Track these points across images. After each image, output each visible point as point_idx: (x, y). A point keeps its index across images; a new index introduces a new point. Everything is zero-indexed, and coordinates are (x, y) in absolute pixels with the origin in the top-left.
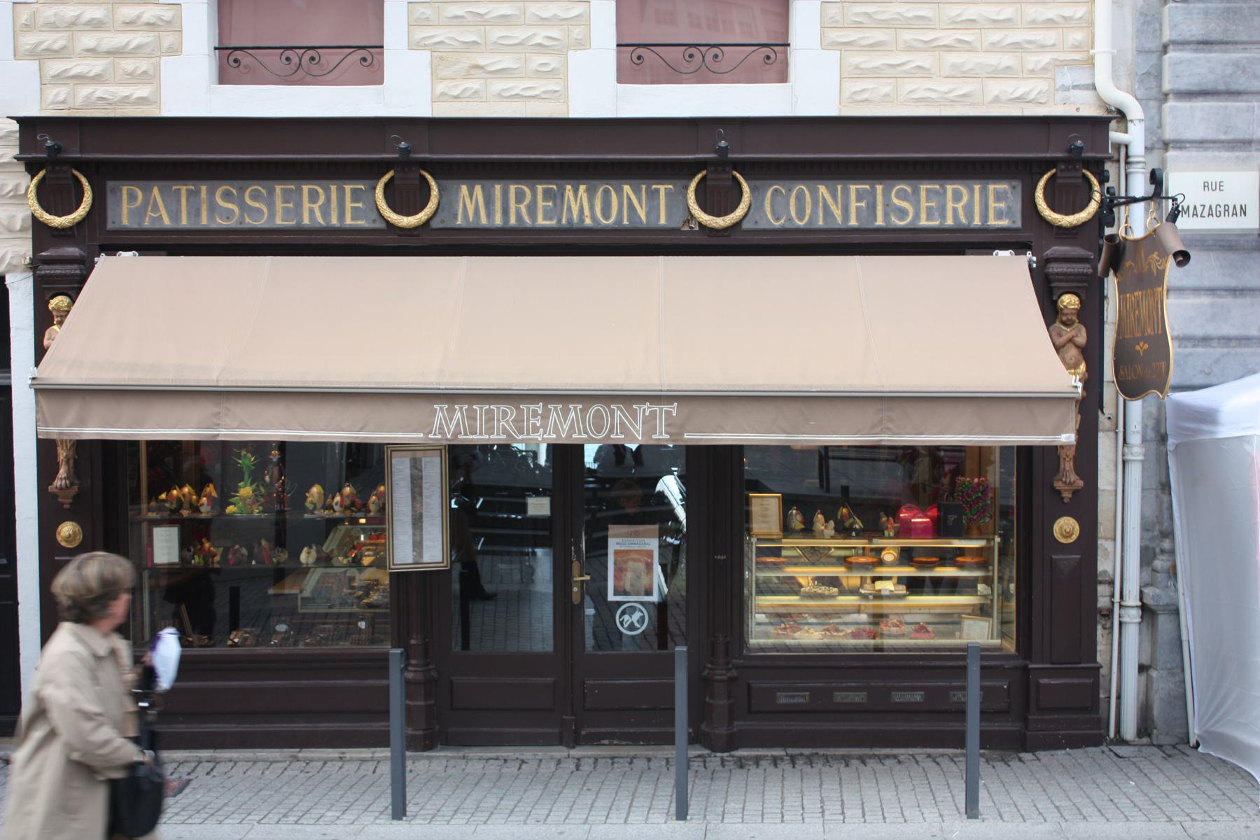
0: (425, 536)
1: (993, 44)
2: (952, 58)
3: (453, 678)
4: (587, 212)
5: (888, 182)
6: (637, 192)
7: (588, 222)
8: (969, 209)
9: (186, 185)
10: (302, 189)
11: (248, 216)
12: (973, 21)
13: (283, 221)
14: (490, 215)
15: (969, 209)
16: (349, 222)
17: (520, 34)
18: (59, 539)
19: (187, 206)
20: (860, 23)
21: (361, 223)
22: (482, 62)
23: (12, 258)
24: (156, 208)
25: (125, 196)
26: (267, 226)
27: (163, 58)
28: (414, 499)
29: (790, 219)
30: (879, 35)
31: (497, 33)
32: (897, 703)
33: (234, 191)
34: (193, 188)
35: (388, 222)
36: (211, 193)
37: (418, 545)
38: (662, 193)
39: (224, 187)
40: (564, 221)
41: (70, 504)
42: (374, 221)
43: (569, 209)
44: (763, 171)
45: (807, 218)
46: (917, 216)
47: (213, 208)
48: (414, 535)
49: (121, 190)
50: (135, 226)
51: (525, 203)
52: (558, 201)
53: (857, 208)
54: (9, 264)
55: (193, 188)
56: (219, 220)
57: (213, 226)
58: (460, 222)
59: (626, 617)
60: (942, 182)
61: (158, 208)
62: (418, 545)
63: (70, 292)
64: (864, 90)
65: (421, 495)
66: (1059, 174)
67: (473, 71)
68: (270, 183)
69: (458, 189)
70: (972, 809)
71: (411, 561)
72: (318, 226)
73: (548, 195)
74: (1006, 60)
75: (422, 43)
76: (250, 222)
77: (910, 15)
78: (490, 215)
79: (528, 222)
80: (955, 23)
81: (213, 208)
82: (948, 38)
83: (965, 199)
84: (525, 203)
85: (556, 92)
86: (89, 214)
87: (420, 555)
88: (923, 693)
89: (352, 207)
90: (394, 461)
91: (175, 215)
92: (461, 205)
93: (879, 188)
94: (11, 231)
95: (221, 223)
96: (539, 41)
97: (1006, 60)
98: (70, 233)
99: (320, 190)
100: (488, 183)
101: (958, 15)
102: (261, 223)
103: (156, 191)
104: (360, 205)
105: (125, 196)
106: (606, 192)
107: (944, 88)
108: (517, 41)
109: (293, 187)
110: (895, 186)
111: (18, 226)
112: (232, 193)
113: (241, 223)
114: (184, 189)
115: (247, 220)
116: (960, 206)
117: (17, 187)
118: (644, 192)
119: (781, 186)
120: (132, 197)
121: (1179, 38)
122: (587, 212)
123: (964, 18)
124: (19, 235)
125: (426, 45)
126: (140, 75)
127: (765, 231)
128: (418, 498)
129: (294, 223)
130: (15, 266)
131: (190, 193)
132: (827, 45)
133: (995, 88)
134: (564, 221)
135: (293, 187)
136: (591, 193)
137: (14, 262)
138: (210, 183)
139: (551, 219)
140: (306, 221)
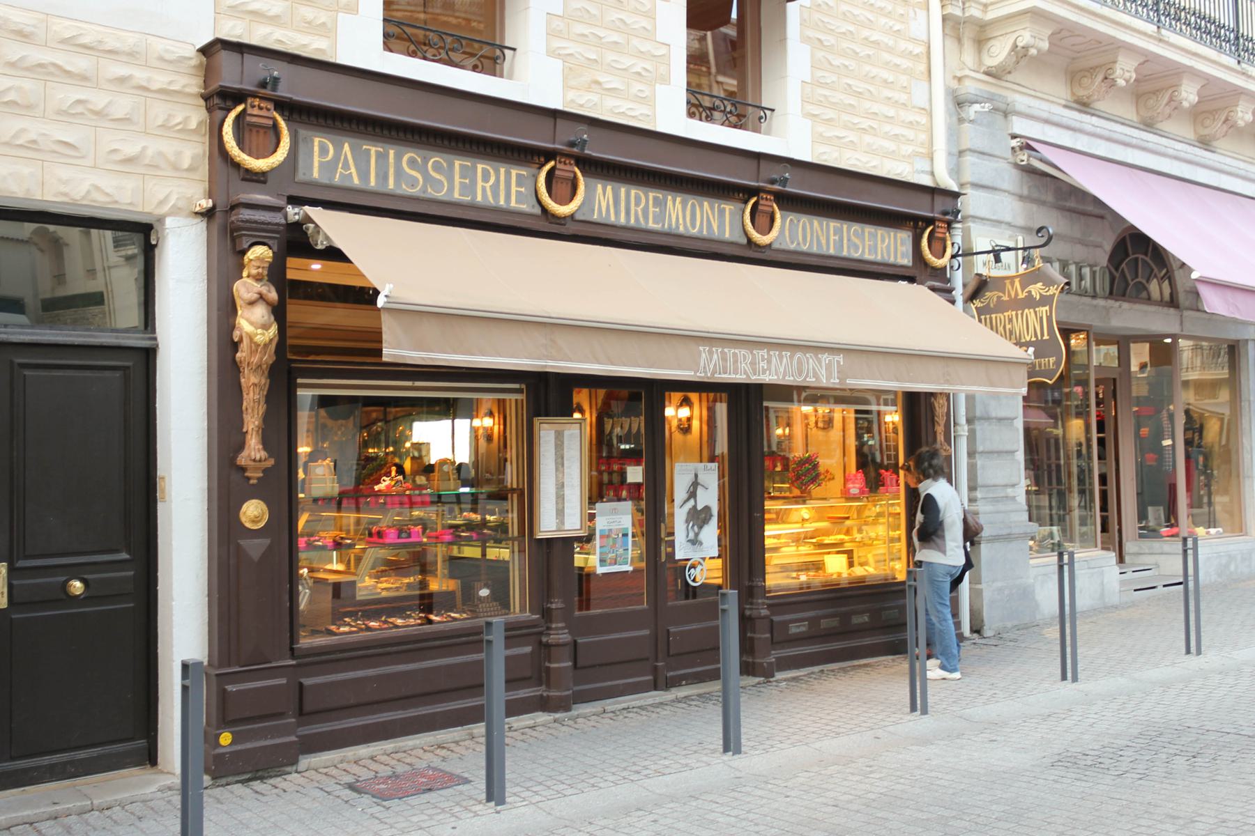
0: (566, 505)
1: (886, 133)
2: (868, 139)
3: (302, 680)
4: (681, 221)
5: (850, 223)
6: (712, 208)
7: (681, 229)
8: (495, 188)
9: (376, 146)
10: (476, 168)
11: (431, 187)
12: (876, 114)
13: (460, 195)
14: (617, 213)
15: (495, 188)
16: (513, 204)
17: (626, 62)
18: (243, 519)
19: (376, 168)
20: (821, 101)
21: (524, 207)
22: (601, 79)
23: (178, 199)
24: (346, 166)
25: (316, 149)
26: (446, 199)
27: (340, 14)
28: (557, 469)
29: (798, 244)
30: (831, 114)
31: (610, 57)
32: (856, 624)
33: (419, 160)
34: (381, 150)
35: (544, 210)
36: (398, 158)
37: (560, 513)
38: (727, 213)
39: (409, 154)
40: (666, 226)
41: (258, 479)
42: (533, 206)
43: (670, 215)
44: (792, 202)
45: (808, 244)
46: (451, 189)
47: (399, 172)
48: (557, 503)
49: (313, 142)
50: (325, 181)
51: (641, 207)
52: (663, 208)
53: (834, 240)
54: (173, 206)
55: (381, 150)
56: (404, 187)
57: (399, 192)
58: (595, 217)
59: (692, 570)
60: (473, 160)
61: (349, 165)
62: (560, 513)
63: (270, 242)
64: (825, 153)
65: (563, 465)
66: (559, 166)
67: (594, 86)
68: (451, 157)
69: (596, 187)
70: (731, 743)
71: (554, 529)
72: (489, 204)
73: (657, 202)
74: (891, 146)
75: (557, 53)
76: (431, 193)
77: (847, 102)
78: (617, 213)
79: (643, 225)
80: (868, 113)
81: (399, 172)
82: (866, 124)
83: (642, 205)
84: (641, 207)
85: (648, 116)
86: (583, 204)
87: (562, 522)
88: (838, 619)
89: (460, 182)
90: (542, 433)
91: (364, 175)
92: (597, 202)
93: (845, 227)
94: (176, 168)
95: (406, 190)
96: (639, 70)
97: (891, 146)
98: (262, 179)
99: (492, 172)
100: (616, 185)
101: (870, 108)
102: (441, 195)
103: (346, 147)
104: (523, 190)
105: (316, 149)
106: (693, 206)
107: (864, 160)
108: (624, 67)
109: (469, 164)
110: (434, 157)
111: (186, 163)
112: (417, 161)
113: (424, 192)
114: (373, 149)
115: (429, 190)
116: (488, 185)
117: (187, 119)
118: (716, 210)
119: (417, 155)
120: (324, 151)
121: (972, 148)
122: (681, 221)
123: (872, 111)
124: (185, 175)
125: (559, 54)
126: (318, 26)
127: (784, 251)
128: (561, 469)
129: (469, 198)
130: (179, 209)
131: (378, 155)
132: (552, 53)
133: (610, 102)
134: (666, 226)
135: (469, 164)
136: (684, 204)
137: (180, 204)
138: (628, 186)
139: (658, 223)
140: (479, 198)
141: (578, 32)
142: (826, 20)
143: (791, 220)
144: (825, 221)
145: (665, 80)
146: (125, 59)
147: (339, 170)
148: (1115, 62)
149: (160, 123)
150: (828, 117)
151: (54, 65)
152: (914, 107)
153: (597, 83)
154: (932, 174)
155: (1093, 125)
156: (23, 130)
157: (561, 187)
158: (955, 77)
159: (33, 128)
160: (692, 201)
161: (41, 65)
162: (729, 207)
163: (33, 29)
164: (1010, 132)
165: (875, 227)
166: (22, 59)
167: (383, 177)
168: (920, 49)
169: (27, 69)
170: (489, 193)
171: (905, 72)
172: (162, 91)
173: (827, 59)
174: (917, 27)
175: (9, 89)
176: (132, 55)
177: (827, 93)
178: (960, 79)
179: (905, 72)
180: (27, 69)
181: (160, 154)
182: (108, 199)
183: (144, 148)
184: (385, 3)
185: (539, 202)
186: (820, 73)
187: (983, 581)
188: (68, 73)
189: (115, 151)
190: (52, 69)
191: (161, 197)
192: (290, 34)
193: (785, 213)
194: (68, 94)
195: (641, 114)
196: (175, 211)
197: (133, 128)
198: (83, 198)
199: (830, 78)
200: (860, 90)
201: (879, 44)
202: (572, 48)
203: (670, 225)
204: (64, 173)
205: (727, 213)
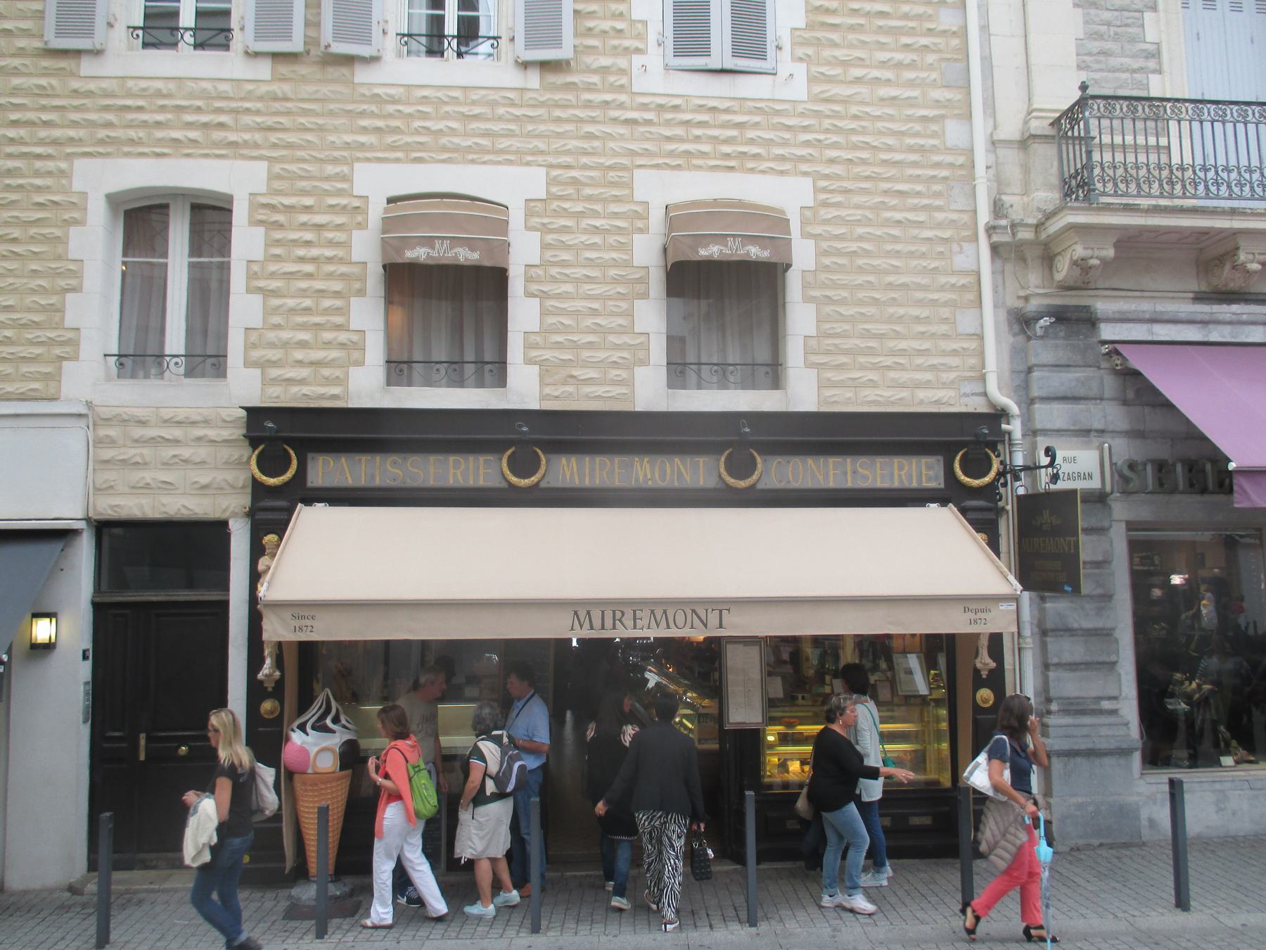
12: (905, 350)
17: (601, 355)
20: (830, 350)
22: (575, 373)
27: (351, 368)
38: (701, 464)
67: (569, 379)
74: (928, 376)
94: (233, 487)
117: (241, 456)
137: (236, 510)
141: (553, 341)
142: (834, 277)
143: (779, 462)
144: (822, 460)
145: (645, 362)
146: (203, 425)
147: (617, 470)
148: (1237, 248)
149: (223, 461)
150: (838, 363)
151: (160, 437)
152: (960, 335)
153: (572, 376)
154: (985, 394)
155: (1234, 314)
156: (143, 478)
157: (524, 466)
158: (1019, 297)
159: (147, 476)
160: (659, 459)
161: (153, 438)
162: (701, 461)
163: (147, 418)
164: (1099, 339)
165: (890, 457)
166: (141, 437)
167: (592, 476)
168: (971, 279)
169: (145, 442)
170: (460, 477)
171: (946, 304)
172: (225, 441)
173: (837, 311)
174: (962, 261)
175: (135, 455)
176: (206, 422)
177: (837, 341)
178: (1026, 298)
179: (946, 304)
180: (145, 442)
181: (225, 480)
182: (191, 513)
183: (214, 478)
184: (677, 8)
185: (720, 476)
186: (827, 326)
187: (1054, 793)
188: (168, 440)
189: (196, 482)
190: (160, 439)
191: (224, 507)
192: (313, 388)
193: (764, 457)
194: (168, 452)
195: (618, 394)
196: (235, 515)
197: (208, 466)
198: (176, 514)
199: (839, 327)
200: (882, 332)
201: (908, 285)
202: (547, 354)
203: (637, 479)
204: (165, 500)
205: (701, 464)
